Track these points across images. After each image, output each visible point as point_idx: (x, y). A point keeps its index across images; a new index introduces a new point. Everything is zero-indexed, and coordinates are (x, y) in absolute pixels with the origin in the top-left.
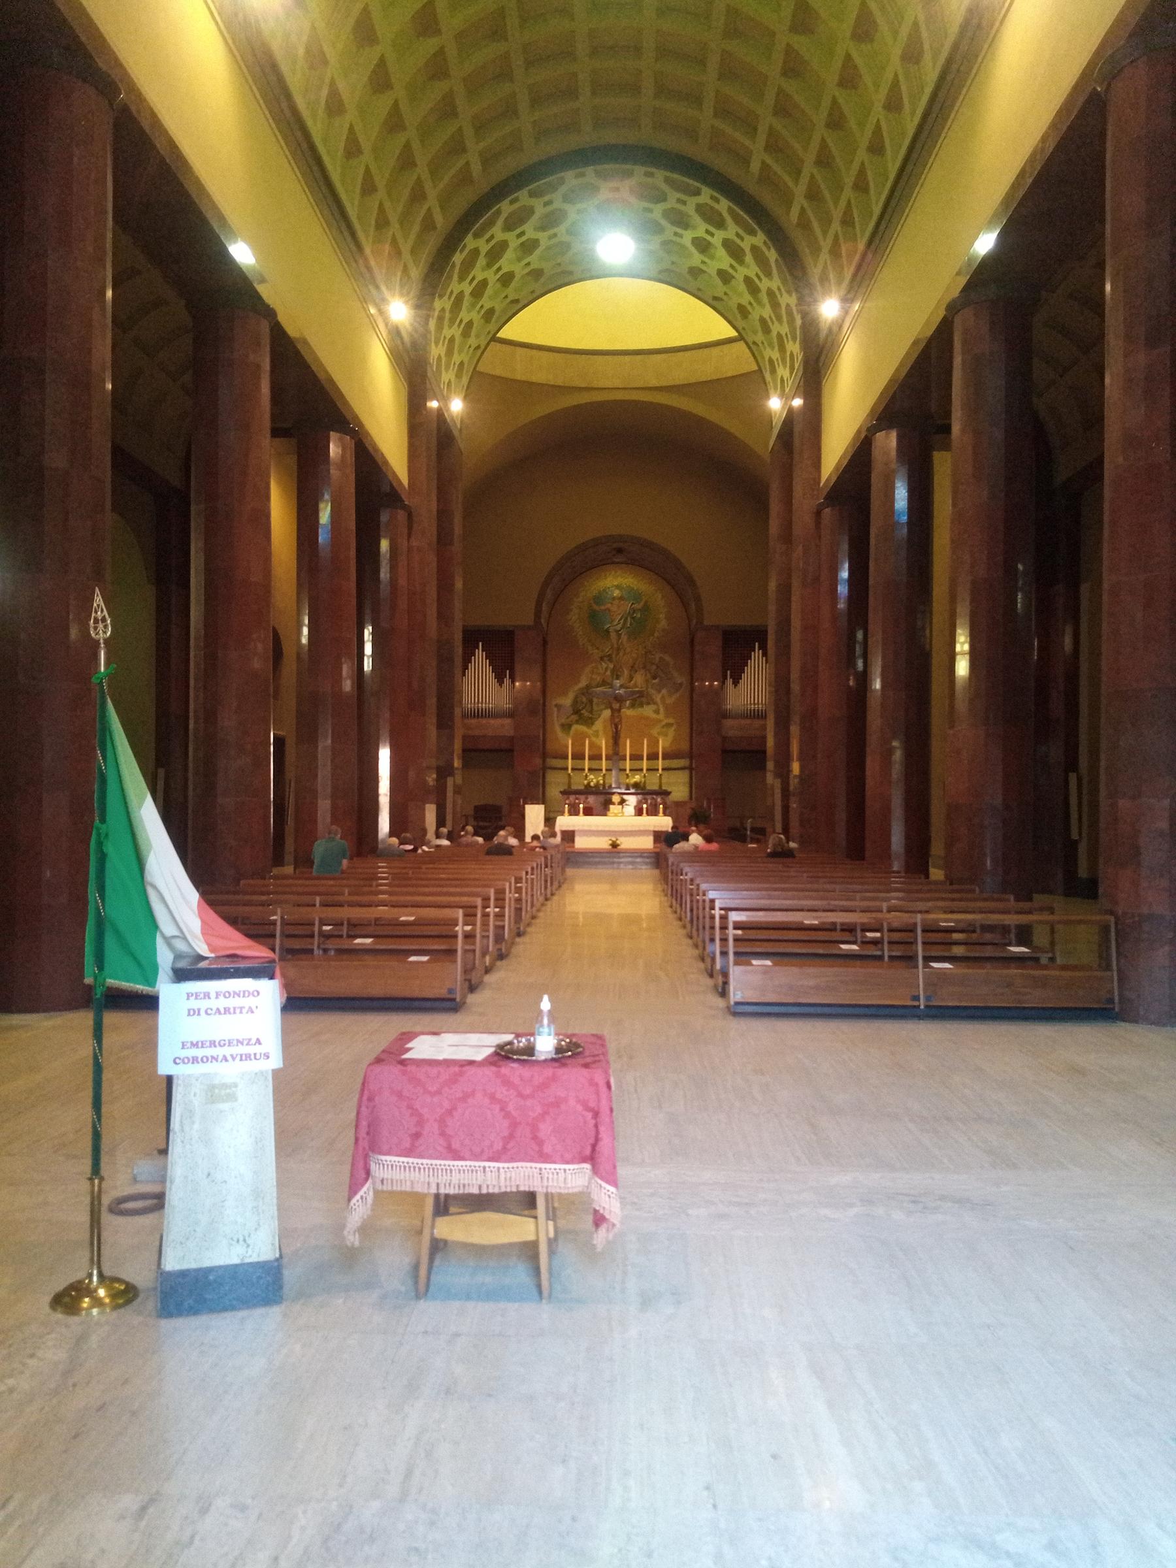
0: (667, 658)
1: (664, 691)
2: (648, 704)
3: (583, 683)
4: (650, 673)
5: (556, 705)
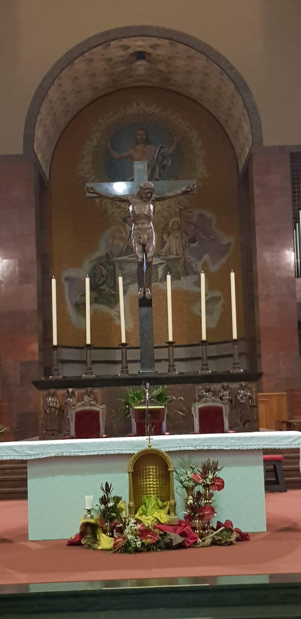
0: (208, 214)
1: (206, 257)
2: (187, 274)
3: (101, 252)
4: (187, 235)
5: (67, 279)
